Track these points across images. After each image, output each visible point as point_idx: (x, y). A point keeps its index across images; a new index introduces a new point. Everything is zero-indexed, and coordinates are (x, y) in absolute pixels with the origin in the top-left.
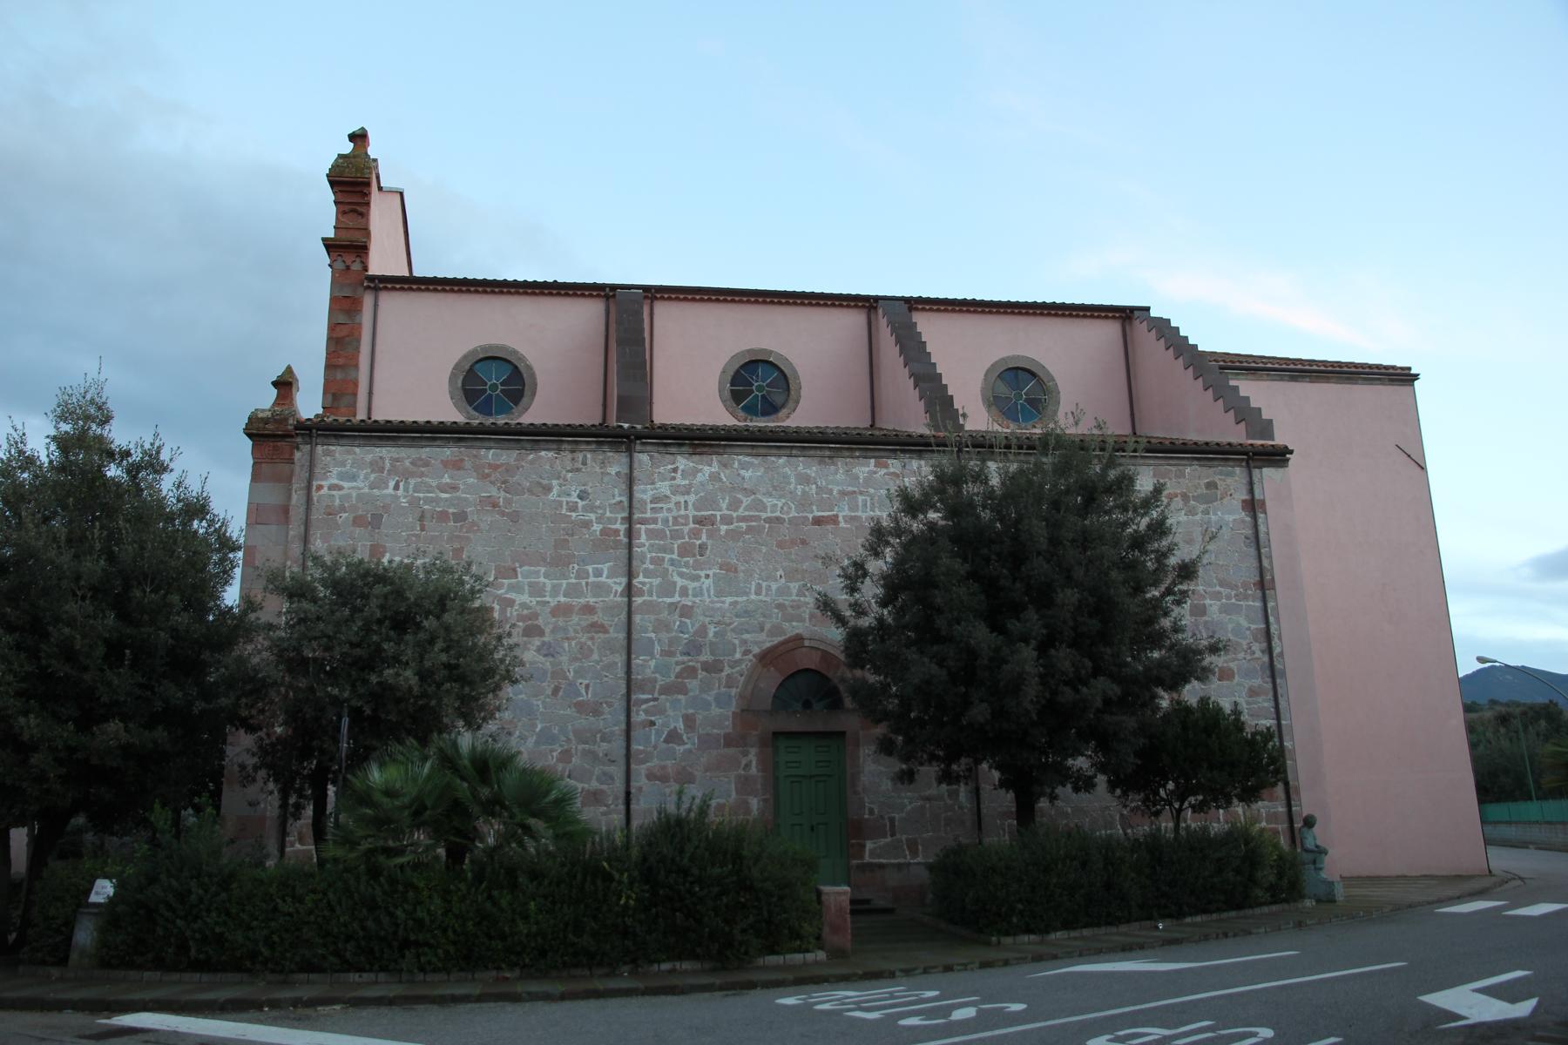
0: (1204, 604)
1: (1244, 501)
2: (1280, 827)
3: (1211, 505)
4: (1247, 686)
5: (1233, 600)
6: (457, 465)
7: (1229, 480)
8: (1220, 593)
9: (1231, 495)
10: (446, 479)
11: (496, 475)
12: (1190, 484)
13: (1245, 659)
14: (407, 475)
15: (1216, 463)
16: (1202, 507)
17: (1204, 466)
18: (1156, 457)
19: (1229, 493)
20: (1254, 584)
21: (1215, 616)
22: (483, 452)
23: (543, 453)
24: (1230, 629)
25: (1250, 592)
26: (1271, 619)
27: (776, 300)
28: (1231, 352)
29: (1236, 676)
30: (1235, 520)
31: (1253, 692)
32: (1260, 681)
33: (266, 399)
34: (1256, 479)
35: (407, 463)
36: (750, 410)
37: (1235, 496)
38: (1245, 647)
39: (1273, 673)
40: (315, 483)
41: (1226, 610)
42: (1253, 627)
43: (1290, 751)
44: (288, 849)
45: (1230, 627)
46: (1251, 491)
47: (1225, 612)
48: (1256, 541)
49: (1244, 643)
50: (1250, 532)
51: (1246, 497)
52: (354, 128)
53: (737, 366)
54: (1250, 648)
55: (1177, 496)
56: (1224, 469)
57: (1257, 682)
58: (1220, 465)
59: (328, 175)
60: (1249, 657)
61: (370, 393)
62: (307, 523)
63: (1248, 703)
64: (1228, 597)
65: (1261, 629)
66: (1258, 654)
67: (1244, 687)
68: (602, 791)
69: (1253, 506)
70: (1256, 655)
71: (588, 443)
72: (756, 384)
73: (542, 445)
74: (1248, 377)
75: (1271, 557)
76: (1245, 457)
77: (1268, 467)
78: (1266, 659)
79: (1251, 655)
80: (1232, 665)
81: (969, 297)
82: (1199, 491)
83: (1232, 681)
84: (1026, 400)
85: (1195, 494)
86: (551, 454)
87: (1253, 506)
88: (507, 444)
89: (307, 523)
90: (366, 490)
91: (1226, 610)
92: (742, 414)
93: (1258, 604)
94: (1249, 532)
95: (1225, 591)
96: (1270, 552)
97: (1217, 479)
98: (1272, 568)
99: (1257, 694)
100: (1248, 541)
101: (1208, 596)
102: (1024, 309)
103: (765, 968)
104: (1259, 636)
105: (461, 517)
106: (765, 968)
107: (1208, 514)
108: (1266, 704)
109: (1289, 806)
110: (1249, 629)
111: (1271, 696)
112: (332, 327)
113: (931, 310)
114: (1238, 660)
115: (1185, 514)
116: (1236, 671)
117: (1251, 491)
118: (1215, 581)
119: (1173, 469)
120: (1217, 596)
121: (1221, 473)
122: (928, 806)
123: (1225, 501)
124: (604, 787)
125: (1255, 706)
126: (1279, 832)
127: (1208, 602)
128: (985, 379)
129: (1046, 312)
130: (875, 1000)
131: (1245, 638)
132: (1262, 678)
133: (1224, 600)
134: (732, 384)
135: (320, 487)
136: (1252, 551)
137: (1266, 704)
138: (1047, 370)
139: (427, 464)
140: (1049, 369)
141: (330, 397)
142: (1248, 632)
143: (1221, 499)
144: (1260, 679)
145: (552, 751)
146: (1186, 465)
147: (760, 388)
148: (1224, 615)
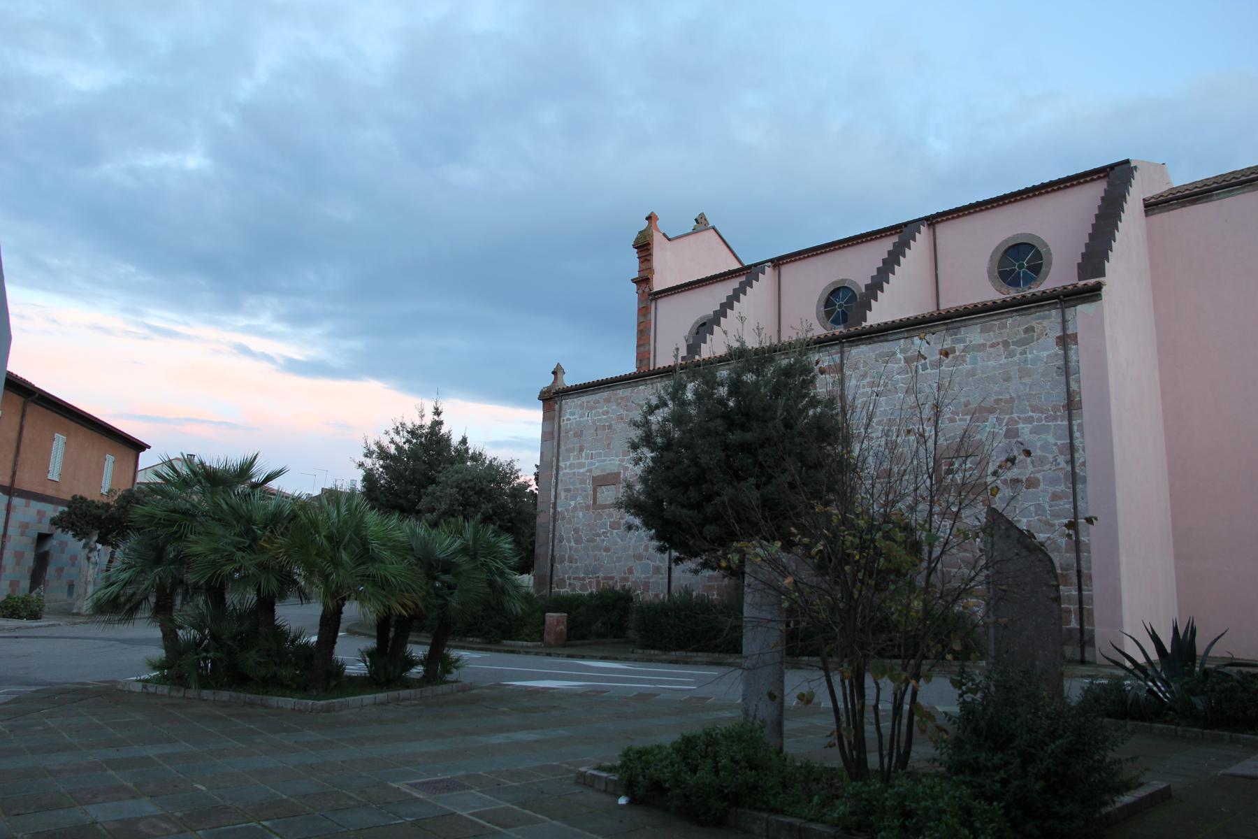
0: (1018, 428)
1: (1058, 338)
2: (1072, 608)
3: (1028, 346)
4: (1050, 491)
5: (1044, 422)
6: (608, 401)
7: (1046, 323)
8: (1032, 417)
9: (1046, 335)
10: (605, 409)
11: (623, 403)
12: (1011, 333)
13: (1050, 469)
14: (591, 408)
15: (1033, 310)
16: (1020, 349)
17: (1022, 315)
18: (980, 317)
19: (1045, 333)
20: (1063, 407)
21: (1026, 437)
22: (618, 391)
23: (640, 387)
24: (1038, 447)
25: (1059, 414)
26: (1077, 434)
27: (944, 219)
28: (1224, 173)
29: (1041, 484)
30: (1048, 355)
31: (1055, 497)
32: (1063, 488)
33: (548, 381)
34: (1068, 317)
35: (592, 402)
36: (836, 322)
37: (1049, 335)
38: (1051, 460)
39: (1074, 478)
40: (562, 419)
41: (1035, 431)
42: (1059, 442)
43: (1086, 544)
44: (553, 591)
45: (1039, 444)
46: (1064, 329)
47: (1035, 432)
48: (1067, 370)
49: (1050, 457)
50: (1062, 363)
51: (1060, 333)
52: (647, 215)
53: (827, 294)
54: (1056, 460)
55: (999, 344)
56: (1042, 313)
57: (1060, 488)
58: (1036, 312)
59: (633, 245)
60: (1053, 468)
61: (655, 356)
62: (559, 440)
63: (1051, 506)
64: (1039, 420)
65: (1067, 443)
66: (1063, 465)
67: (1048, 492)
68: (661, 567)
69: (1066, 340)
70: (1061, 466)
71: (657, 378)
72: (838, 304)
73: (640, 383)
74: (1246, 190)
75: (1080, 381)
76: (1057, 300)
77: (1082, 303)
78: (1069, 468)
79: (1056, 466)
80: (1038, 475)
81: (1030, 186)
82: (1018, 337)
83: (1037, 488)
84: (1028, 268)
85: (1015, 340)
86: (644, 387)
87: (1066, 340)
88: (626, 386)
89: (559, 440)
90: (578, 419)
91: (1035, 431)
92: (829, 325)
93: (1066, 423)
94: (1061, 363)
95: (1035, 415)
96: (1079, 377)
97: (1034, 324)
98: (1080, 391)
99: (1060, 498)
100: (1060, 371)
101: (1021, 421)
102: (1081, 179)
103: (505, 645)
104: (1065, 449)
105: (610, 427)
106: (505, 645)
107: (1026, 353)
108: (1067, 506)
109: (1080, 590)
110: (1056, 444)
111: (1071, 500)
112: (639, 324)
113: (948, 219)
114: (1044, 471)
115: (1005, 358)
116: (1041, 480)
117: (1064, 329)
118: (1028, 408)
119: (997, 323)
120: (1029, 420)
121: (1039, 318)
122: (815, 580)
123: (1041, 341)
124: (661, 564)
125: (1057, 508)
126: (1071, 611)
127: (1021, 426)
128: (991, 260)
129: (1012, 200)
130: (639, 681)
131: (1051, 452)
132: (1065, 484)
133: (1035, 423)
134: (825, 308)
135: (564, 420)
136: (1063, 379)
137: (1067, 506)
138: (1042, 239)
139: (598, 402)
140: (1044, 239)
141: (639, 363)
142: (1054, 447)
143: (1038, 339)
144: (1063, 486)
145: (641, 545)
146: (1006, 318)
147: (840, 306)
148: (1034, 435)
